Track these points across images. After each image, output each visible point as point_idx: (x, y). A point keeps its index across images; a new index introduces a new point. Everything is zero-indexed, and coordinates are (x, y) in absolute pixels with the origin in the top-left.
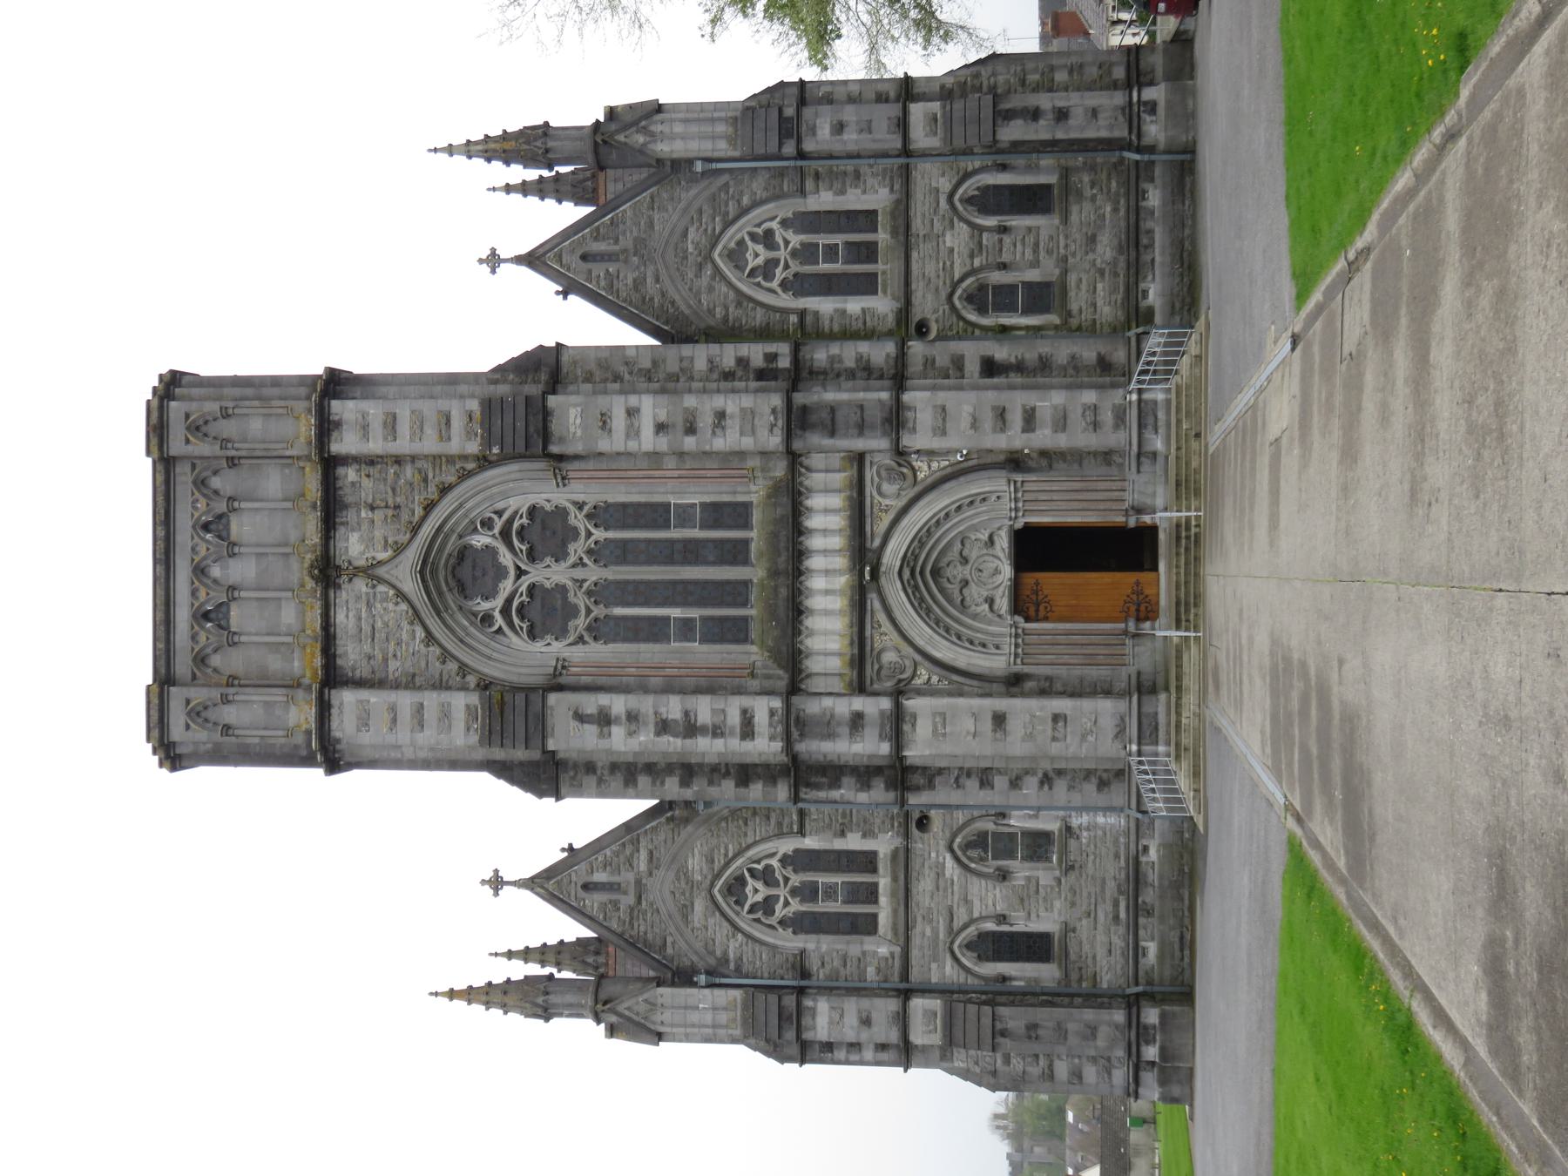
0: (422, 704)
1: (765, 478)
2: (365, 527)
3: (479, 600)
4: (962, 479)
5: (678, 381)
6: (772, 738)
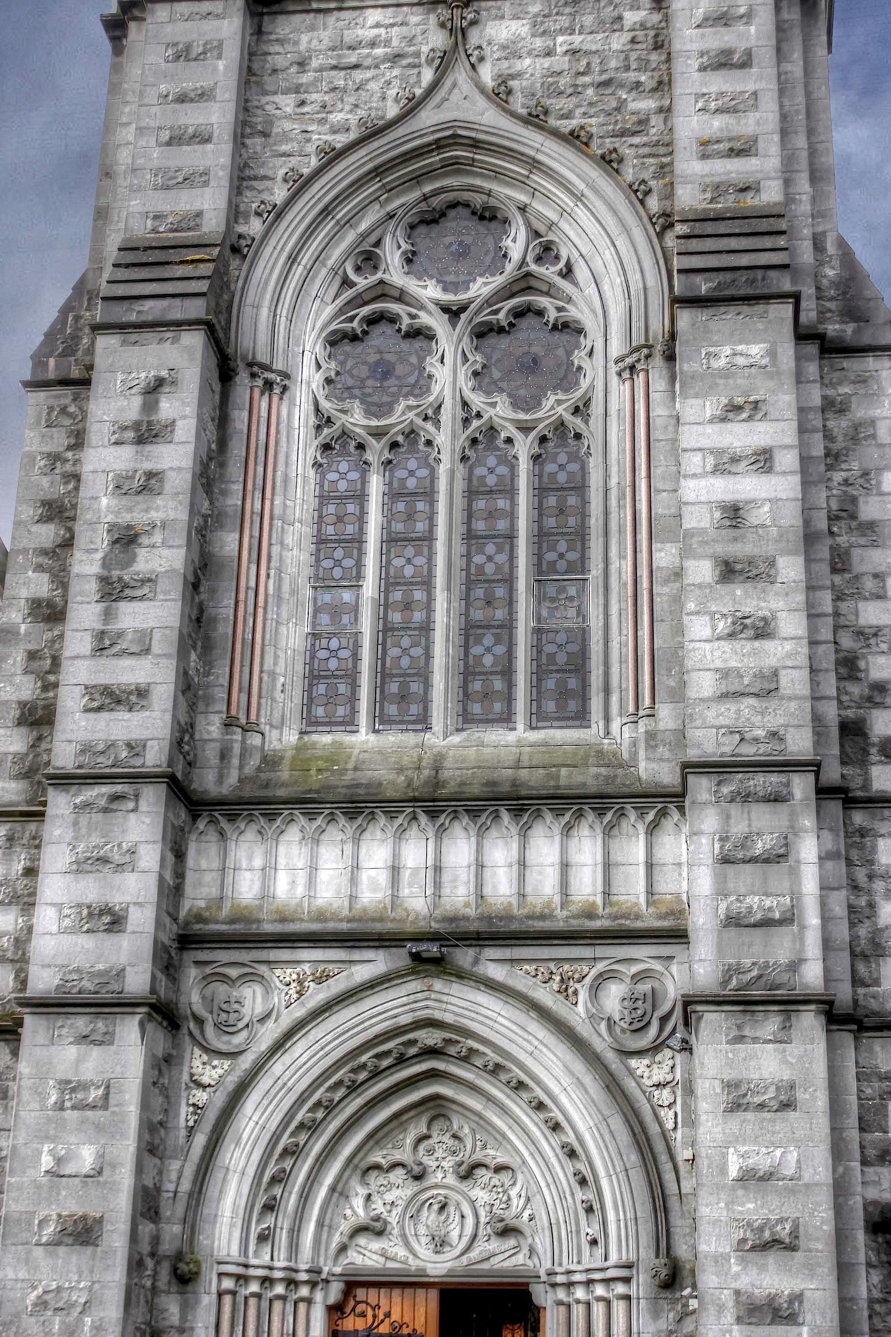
0: (208, 140)
1: (634, 743)
2: (539, 43)
3: (404, 246)
4: (633, 1158)
5: (834, 570)
6: (86, 749)
